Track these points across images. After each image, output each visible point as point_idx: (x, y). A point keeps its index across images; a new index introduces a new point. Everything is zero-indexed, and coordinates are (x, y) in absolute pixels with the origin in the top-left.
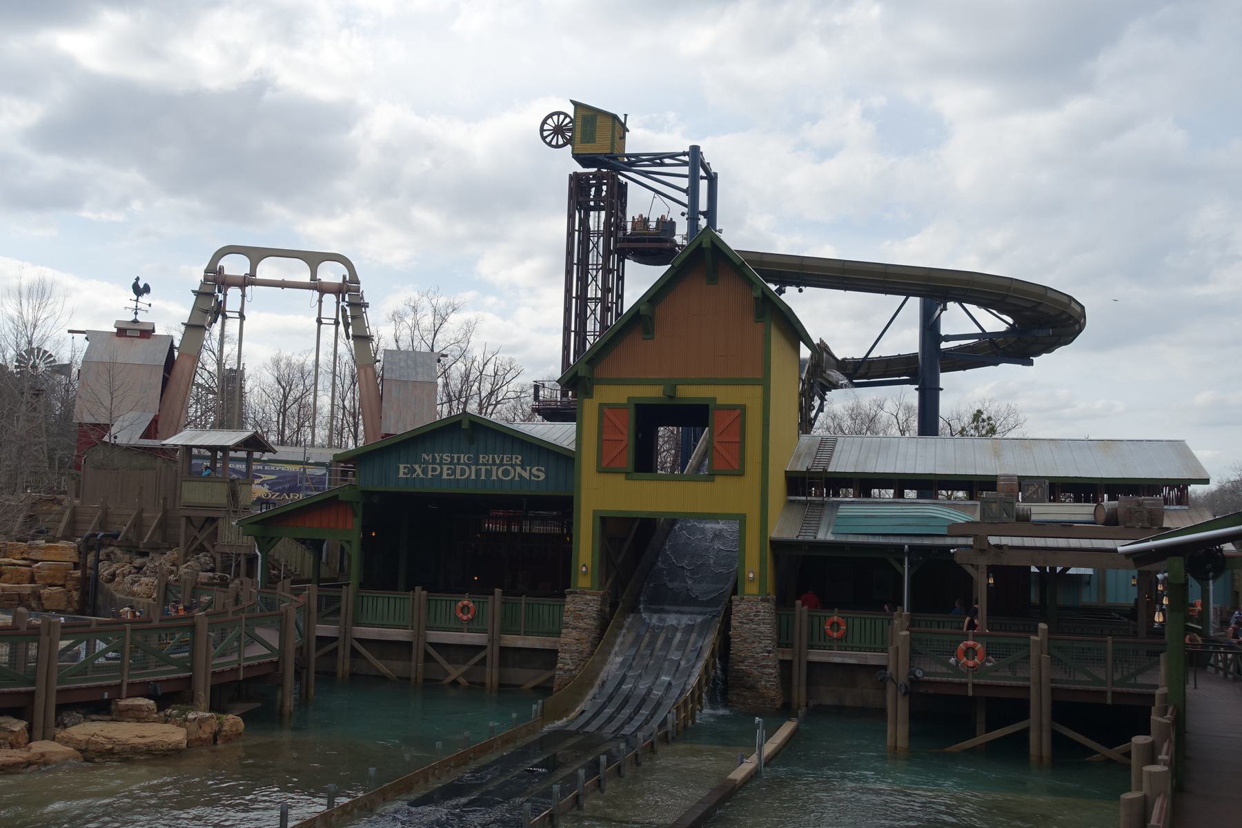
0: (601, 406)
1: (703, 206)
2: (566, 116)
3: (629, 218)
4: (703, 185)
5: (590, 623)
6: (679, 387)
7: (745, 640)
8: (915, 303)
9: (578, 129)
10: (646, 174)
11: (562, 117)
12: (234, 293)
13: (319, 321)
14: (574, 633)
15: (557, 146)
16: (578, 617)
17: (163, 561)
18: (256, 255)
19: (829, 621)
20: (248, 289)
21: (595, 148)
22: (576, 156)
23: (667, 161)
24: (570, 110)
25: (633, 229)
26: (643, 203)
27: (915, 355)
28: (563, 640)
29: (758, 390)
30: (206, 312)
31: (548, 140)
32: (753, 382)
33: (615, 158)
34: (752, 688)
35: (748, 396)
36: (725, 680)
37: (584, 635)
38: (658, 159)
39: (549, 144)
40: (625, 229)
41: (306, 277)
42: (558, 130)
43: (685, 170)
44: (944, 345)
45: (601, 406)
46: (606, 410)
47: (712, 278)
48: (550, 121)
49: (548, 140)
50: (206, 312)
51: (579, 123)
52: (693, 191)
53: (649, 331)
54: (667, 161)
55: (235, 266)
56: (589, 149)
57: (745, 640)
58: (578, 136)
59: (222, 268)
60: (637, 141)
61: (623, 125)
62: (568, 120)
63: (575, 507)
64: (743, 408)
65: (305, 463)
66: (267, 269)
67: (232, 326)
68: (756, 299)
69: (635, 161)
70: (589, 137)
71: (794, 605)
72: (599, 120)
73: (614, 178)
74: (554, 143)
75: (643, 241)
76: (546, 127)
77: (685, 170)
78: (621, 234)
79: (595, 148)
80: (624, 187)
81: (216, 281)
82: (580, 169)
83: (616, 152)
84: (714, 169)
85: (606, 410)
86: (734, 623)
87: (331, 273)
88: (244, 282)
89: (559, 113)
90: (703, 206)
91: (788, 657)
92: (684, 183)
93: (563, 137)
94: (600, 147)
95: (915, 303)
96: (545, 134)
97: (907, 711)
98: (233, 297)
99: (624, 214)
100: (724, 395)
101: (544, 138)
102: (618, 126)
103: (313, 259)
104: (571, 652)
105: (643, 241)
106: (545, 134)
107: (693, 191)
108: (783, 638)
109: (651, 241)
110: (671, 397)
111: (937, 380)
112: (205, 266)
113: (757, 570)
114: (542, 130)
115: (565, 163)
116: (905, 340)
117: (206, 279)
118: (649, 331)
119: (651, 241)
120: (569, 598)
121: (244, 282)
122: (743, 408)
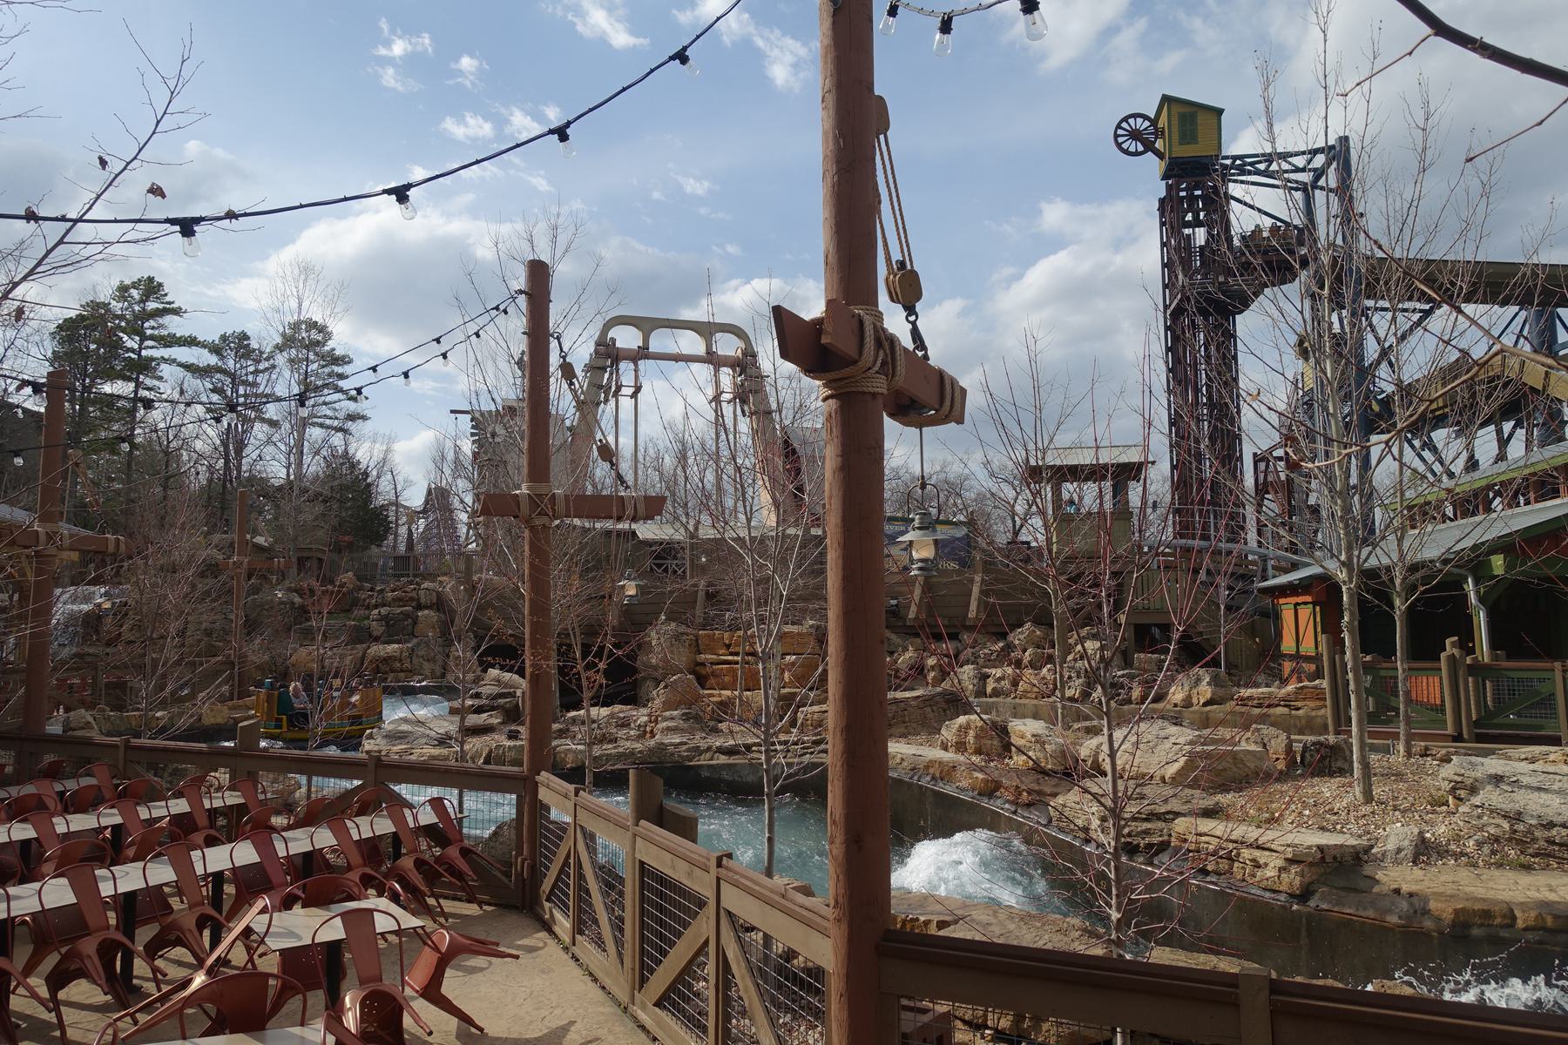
18: (647, 325)
21: (778, 311)
31: (1120, 132)
39: (1116, 136)
41: (700, 349)
49: (1120, 132)
55: (626, 338)
59: (613, 340)
60: (1241, 142)
63: (830, 66)
66: (660, 341)
67: (626, 403)
76: (1131, 121)
79: (778, 311)
81: (608, 355)
87: (728, 346)
88: (642, 353)
96: (1124, 125)
97: (829, 123)
101: (1119, 126)
103: (707, 330)
106: (1124, 125)
114: (1125, 119)
117: (596, 351)
121: (642, 353)
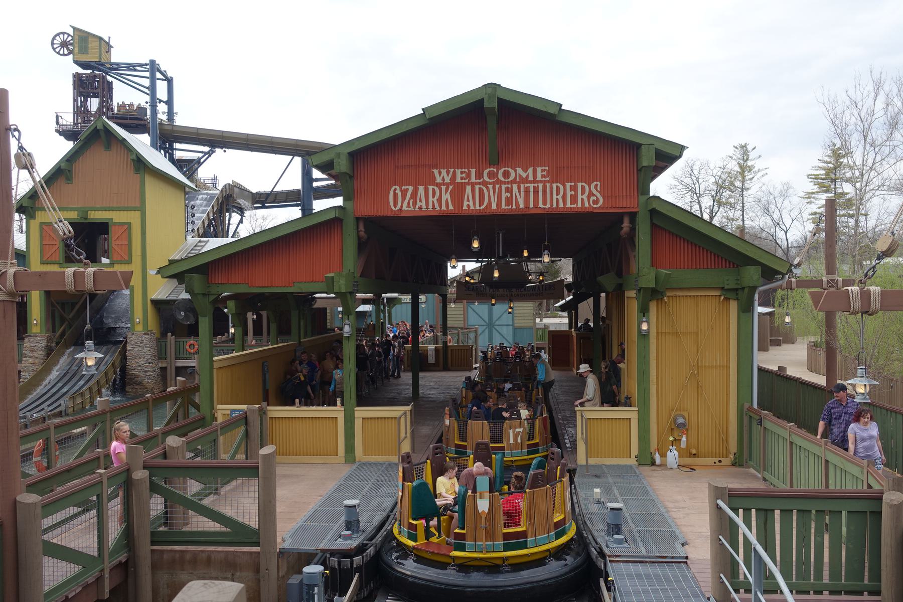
0: (41, 224)
2: (69, 35)
3: (115, 103)
5: (41, 353)
6: (90, 213)
7: (135, 357)
8: (298, 160)
9: (76, 45)
11: (66, 36)
14: (31, 360)
15: (64, 55)
16: (33, 351)
17: (865, 435)
19: (189, 343)
22: (76, 62)
23: (138, 68)
24: (71, 32)
25: (119, 110)
26: (125, 95)
27: (299, 191)
28: (23, 365)
29: (138, 213)
31: (57, 50)
32: (134, 209)
33: (103, 65)
34: (140, 384)
35: (133, 217)
36: (122, 381)
37: (37, 361)
38: (132, 67)
39: (58, 53)
40: (113, 110)
42: (64, 44)
43: (147, 74)
44: (315, 184)
45: (41, 224)
46: (44, 226)
47: (108, 147)
48: (57, 38)
49: (57, 50)
51: (77, 41)
53: (69, 179)
54: (138, 68)
57: (135, 357)
58: (76, 49)
62: (70, 38)
64: (129, 224)
68: (133, 160)
69: (116, 67)
70: (84, 49)
71: (166, 336)
72: (90, 39)
73: (104, 78)
74: (61, 52)
75: (126, 119)
77: (147, 74)
78: (110, 114)
82: (80, 70)
83: (103, 61)
84: (169, 75)
85: (44, 226)
86: (128, 348)
89: (64, 33)
91: (164, 365)
93: (68, 49)
94: (92, 56)
95: (298, 160)
99: (111, 98)
100: (117, 217)
104: (29, 371)
105: (126, 119)
107: (153, 89)
108: (161, 354)
109: (131, 119)
110: (86, 219)
111: (311, 205)
113: (141, 317)
115: (68, 67)
116: (293, 181)
118: (69, 179)
119: (131, 119)
120: (26, 340)
122: (129, 224)
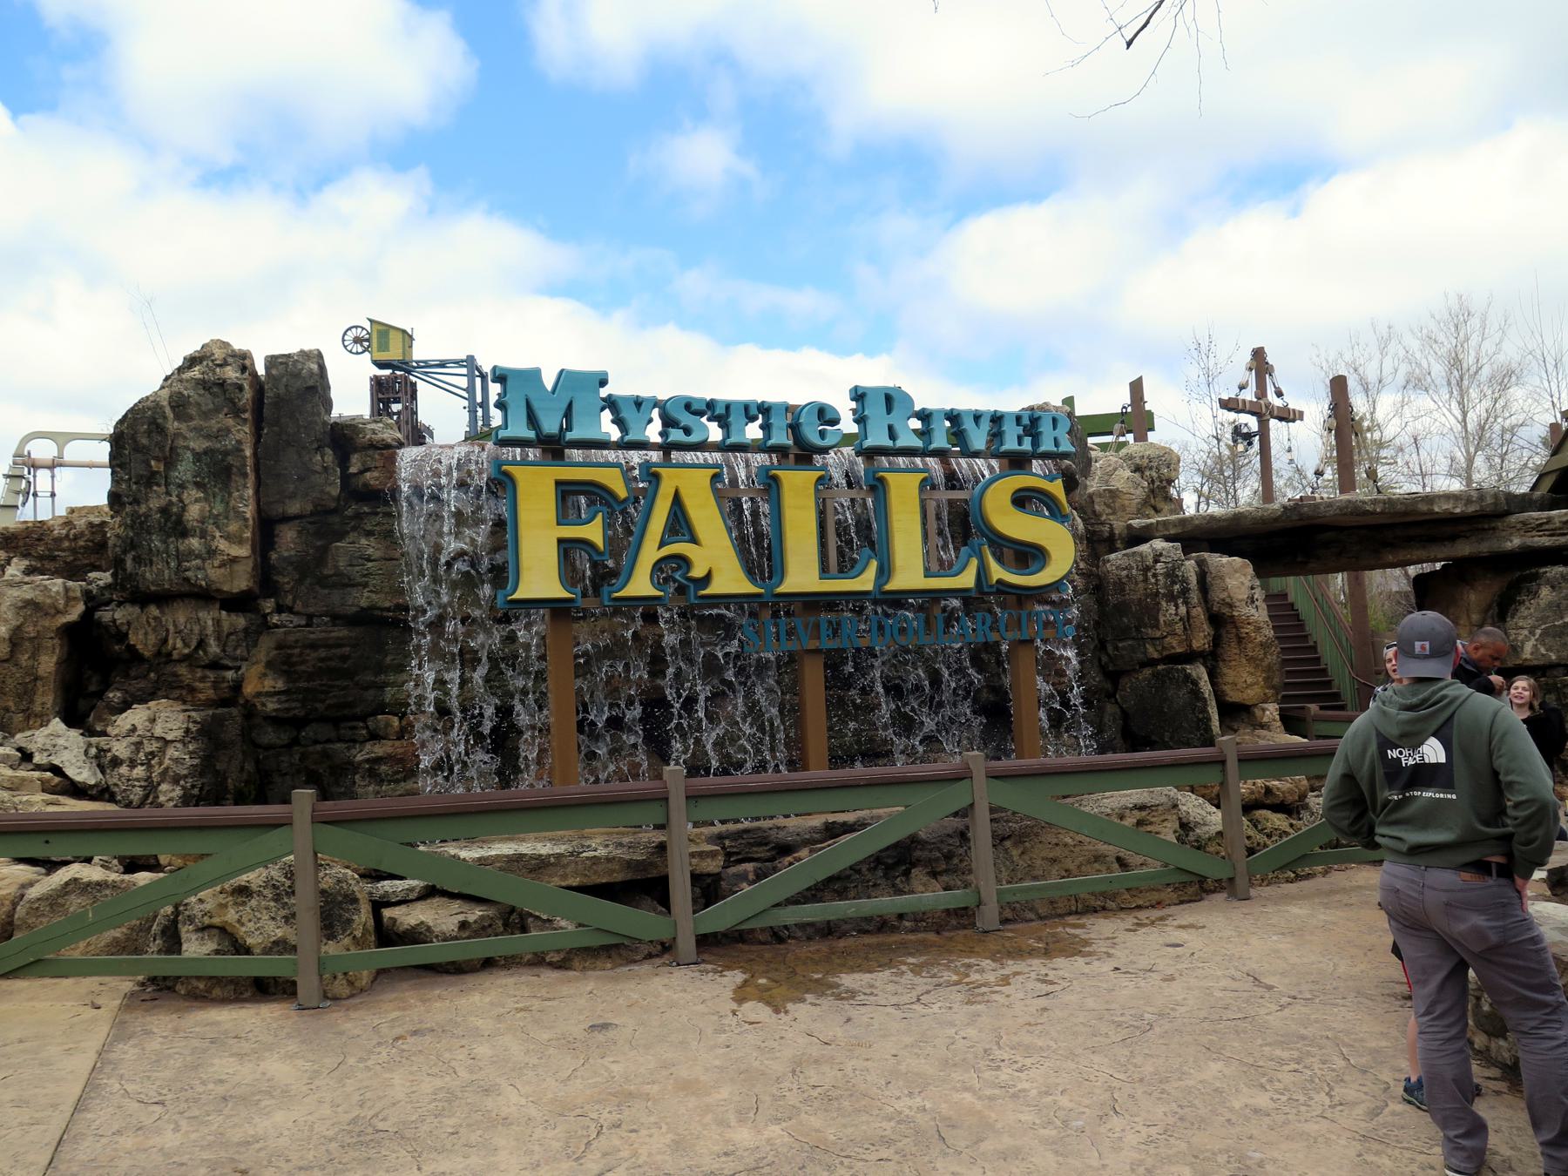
1: (479, 399)
4: (478, 381)
10: (426, 373)
12: (43, 477)
13: (53, 495)
18: (61, 439)
20: (57, 470)
24: (367, 325)
30: (18, 493)
50: (18, 493)
51: (375, 336)
52: (470, 389)
55: (43, 450)
56: (383, 356)
61: (411, 337)
65: (1449, 383)
66: (73, 451)
70: (384, 346)
77: (464, 371)
80: (414, 385)
88: (52, 466)
90: (479, 399)
92: (463, 382)
94: (394, 354)
98: (42, 480)
102: (407, 337)
112: (13, 451)
121: (52, 466)
